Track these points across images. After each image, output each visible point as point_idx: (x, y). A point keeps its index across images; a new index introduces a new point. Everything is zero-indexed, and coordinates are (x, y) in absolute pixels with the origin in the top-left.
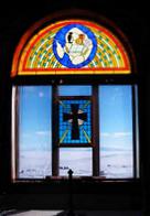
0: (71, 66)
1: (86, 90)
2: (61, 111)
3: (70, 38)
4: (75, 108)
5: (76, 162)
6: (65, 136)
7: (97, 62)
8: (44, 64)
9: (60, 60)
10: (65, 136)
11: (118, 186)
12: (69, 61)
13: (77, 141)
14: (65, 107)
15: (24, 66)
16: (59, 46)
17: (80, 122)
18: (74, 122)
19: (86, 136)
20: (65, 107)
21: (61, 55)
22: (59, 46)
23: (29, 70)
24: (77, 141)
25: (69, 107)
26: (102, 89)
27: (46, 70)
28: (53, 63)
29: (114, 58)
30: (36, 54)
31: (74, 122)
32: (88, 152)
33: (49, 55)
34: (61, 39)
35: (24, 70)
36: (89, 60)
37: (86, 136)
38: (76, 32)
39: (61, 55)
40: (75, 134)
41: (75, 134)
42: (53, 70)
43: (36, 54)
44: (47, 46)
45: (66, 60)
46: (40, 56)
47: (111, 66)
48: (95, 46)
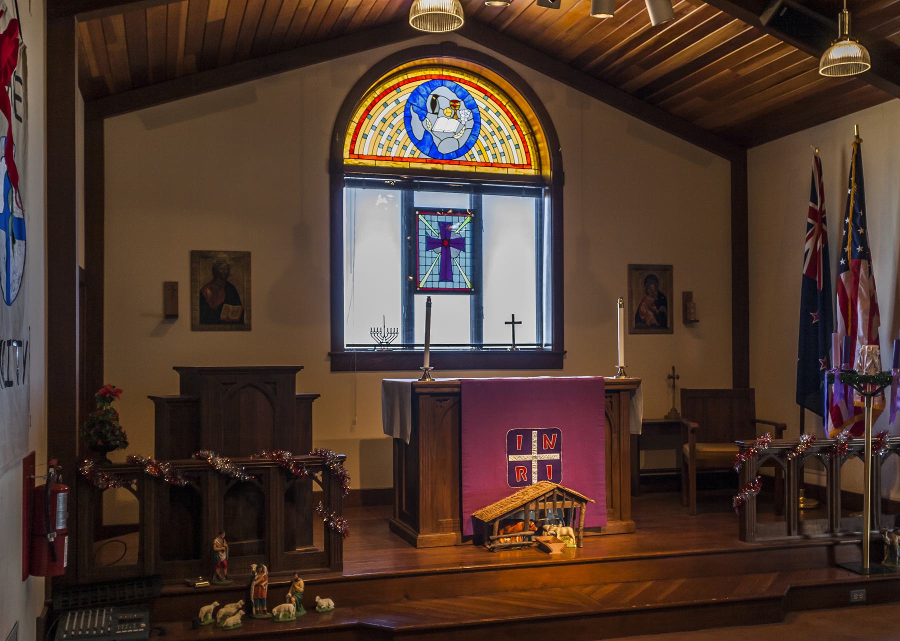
0: (436, 156)
1: (463, 201)
2: (422, 233)
3: (434, 104)
4: (445, 228)
5: (448, 323)
6: (430, 261)
7: (480, 153)
8: (389, 149)
9: (419, 144)
10: (429, 275)
11: (547, 353)
12: (433, 147)
13: (442, 219)
14: (428, 226)
15: (352, 151)
16: (415, 117)
17: (454, 251)
18: (441, 255)
19: (462, 276)
20: (428, 226)
21: (419, 136)
22: (415, 117)
23: (359, 157)
24: (449, 285)
25: (435, 225)
26: (466, 300)
27: (394, 159)
28: (405, 147)
29: (504, 142)
30: (373, 127)
31: (441, 255)
32: (466, 300)
33: (398, 131)
34: (419, 107)
35: (518, 469)
36: (467, 147)
37: (462, 276)
38: (445, 94)
39: (419, 136)
40: (446, 273)
41: (446, 273)
42: (401, 159)
43: (373, 127)
44: (395, 115)
45: (426, 143)
46: (381, 133)
47: (504, 160)
48: (476, 119)
